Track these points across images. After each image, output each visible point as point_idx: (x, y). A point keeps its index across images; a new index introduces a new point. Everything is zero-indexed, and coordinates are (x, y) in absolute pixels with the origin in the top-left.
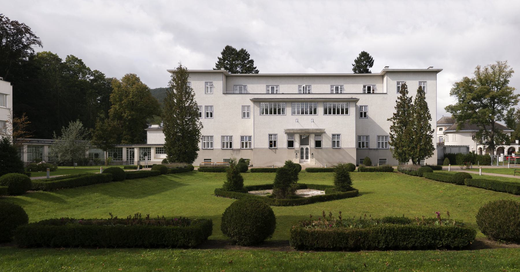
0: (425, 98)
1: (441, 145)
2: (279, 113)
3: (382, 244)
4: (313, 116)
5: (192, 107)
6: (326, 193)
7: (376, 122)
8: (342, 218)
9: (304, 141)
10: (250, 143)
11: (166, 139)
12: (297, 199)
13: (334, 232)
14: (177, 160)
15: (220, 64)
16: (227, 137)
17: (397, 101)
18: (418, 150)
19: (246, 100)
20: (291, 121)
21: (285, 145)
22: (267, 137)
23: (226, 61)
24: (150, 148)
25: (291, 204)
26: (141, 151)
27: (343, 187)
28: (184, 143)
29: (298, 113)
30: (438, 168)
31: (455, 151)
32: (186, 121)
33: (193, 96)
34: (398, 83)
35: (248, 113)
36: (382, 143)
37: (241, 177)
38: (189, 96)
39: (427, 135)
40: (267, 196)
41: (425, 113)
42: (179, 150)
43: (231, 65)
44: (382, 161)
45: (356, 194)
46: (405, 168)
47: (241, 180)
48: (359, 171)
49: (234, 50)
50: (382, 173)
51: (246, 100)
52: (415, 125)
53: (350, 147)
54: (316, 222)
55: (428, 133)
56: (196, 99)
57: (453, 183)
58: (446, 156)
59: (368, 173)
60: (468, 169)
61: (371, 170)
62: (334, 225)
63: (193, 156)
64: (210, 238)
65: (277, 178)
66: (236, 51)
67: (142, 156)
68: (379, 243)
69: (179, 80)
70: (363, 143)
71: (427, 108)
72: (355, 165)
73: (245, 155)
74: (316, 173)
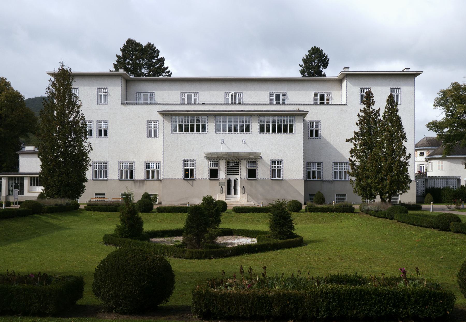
0: (397, 111)
1: (421, 175)
2: (198, 131)
3: (322, 313)
4: (244, 136)
5: (78, 121)
6: (258, 241)
7: (332, 144)
8: (268, 275)
9: (232, 169)
10: (158, 172)
11: (42, 166)
12: (216, 250)
13: (253, 295)
14: (57, 194)
15: (121, 63)
16: (127, 163)
17: (359, 115)
18: (388, 182)
19: (153, 113)
20: (216, 141)
21: (206, 175)
22: (182, 163)
23: (128, 61)
24: (22, 178)
25: (208, 256)
26: (11, 183)
27: (281, 233)
28: (67, 171)
29: (224, 131)
30: (416, 207)
31: (441, 185)
32: (69, 142)
33: (79, 107)
34: (362, 90)
35: (155, 131)
36: (340, 172)
37: (140, 218)
38: (74, 107)
39: (400, 162)
40: (174, 246)
41: (398, 131)
42: (59, 181)
43: (134, 64)
44: (340, 197)
45: (300, 243)
46: (369, 207)
47: (140, 223)
48: (306, 211)
49: (138, 45)
50: (338, 214)
51: (153, 113)
52: (384, 148)
54: (231, 281)
55: (402, 159)
56: (83, 111)
57: (434, 228)
58: (428, 191)
59: (319, 214)
60: (459, 209)
61: (323, 210)
62: (255, 286)
63: (78, 188)
64: (79, 302)
65: (190, 220)
66: (141, 46)
67: (11, 189)
68: (318, 311)
69: (60, 86)
70: (314, 172)
71: (401, 125)
72: (303, 203)
73: (151, 188)
74: (247, 214)
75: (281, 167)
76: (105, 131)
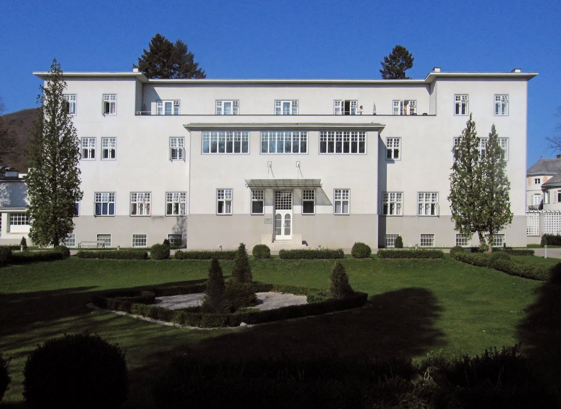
4: (300, 156)
19: (176, 126)
21: (247, 208)
22: (214, 194)
53: (211, 213)
75: (347, 198)
76: (113, 152)
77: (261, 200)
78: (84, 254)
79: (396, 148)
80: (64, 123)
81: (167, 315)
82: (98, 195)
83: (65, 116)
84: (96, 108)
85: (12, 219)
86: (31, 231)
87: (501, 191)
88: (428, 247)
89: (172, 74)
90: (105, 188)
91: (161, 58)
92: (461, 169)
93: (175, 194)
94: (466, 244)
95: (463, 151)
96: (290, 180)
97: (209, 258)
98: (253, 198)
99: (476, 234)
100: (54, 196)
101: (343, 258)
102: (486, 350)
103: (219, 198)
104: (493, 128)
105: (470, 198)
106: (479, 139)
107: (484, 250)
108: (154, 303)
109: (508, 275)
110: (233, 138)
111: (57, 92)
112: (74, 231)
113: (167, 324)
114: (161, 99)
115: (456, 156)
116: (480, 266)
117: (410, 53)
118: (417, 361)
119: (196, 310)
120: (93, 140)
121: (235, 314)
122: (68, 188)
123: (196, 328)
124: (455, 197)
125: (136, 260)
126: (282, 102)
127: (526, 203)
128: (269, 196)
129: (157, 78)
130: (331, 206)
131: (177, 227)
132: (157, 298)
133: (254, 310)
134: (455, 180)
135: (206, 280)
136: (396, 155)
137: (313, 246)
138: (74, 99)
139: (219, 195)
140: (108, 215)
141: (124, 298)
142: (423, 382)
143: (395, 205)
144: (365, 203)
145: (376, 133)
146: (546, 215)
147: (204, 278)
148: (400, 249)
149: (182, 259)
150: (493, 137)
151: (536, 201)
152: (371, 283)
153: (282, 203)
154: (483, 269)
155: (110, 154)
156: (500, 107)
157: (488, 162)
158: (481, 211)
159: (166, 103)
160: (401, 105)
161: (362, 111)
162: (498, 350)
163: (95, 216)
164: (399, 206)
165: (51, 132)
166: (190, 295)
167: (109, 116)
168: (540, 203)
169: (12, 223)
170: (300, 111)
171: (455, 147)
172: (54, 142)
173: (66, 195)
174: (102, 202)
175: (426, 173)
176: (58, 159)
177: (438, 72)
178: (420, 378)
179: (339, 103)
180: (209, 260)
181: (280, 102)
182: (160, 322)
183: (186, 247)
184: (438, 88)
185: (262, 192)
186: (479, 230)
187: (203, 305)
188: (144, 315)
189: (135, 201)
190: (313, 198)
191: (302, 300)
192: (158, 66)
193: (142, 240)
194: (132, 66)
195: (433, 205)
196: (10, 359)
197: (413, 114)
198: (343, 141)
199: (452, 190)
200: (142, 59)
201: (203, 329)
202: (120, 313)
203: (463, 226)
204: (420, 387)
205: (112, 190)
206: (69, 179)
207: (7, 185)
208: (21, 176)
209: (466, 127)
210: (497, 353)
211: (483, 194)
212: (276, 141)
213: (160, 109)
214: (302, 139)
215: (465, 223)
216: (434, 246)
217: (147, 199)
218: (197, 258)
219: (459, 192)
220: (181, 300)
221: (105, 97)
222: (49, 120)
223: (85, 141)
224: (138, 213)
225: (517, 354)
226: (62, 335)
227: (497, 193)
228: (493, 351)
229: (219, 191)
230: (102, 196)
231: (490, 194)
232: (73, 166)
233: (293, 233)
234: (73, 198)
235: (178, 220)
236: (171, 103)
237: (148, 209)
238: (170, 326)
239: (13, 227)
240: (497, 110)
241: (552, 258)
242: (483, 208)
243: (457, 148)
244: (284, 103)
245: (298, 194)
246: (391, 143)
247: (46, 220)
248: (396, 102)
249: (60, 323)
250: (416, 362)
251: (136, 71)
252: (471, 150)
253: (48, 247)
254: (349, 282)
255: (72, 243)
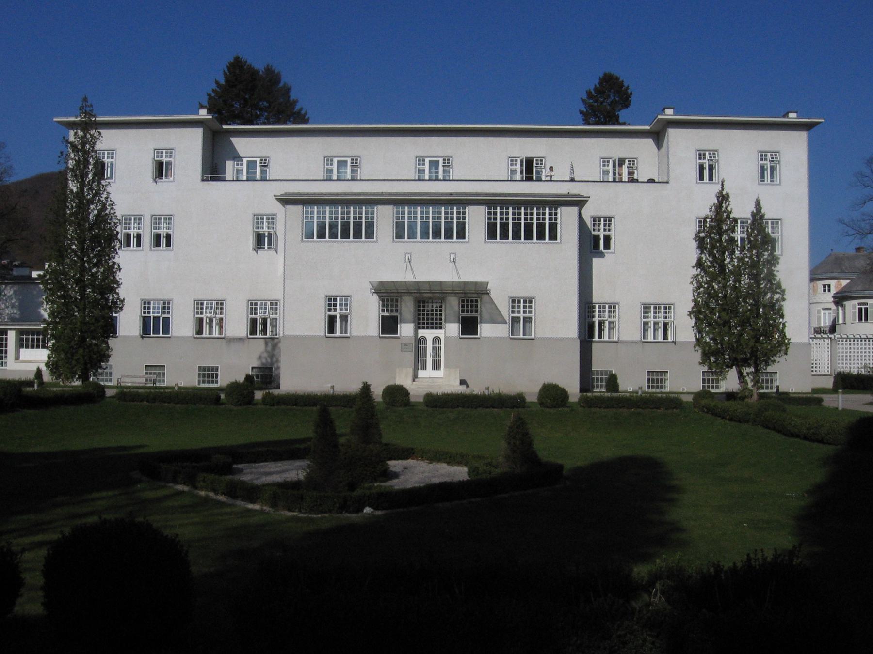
4: (454, 246)
19: (263, 197)
21: (373, 327)
22: (322, 304)
75: (530, 312)
76: (168, 237)
77: (394, 314)
78: (127, 395)
79: (607, 233)
80: (98, 194)
81: (251, 493)
82: (146, 305)
83: (99, 183)
84: (145, 171)
85: (22, 340)
86: (49, 358)
87: (771, 302)
88: (658, 391)
89: (258, 117)
90: (157, 293)
91: (242, 93)
92: (710, 267)
93: (261, 304)
94: (717, 387)
95: (712, 239)
96: (441, 283)
97: (315, 405)
98: (383, 311)
99: (733, 373)
100: (81, 306)
101: (524, 407)
102: (748, 555)
103: (330, 310)
104: (758, 204)
105: (723, 314)
106: (735, 220)
107: (746, 397)
108: (231, 474)
109: (784, 437)
110: (352, 215)
111: (88, 146)
112: (110, 359)
113: (251, 506)
114: (241, 155)
115: (701, 246)
116: (739, 422)
117: (626, 84)
118: (641, 571)
119: (295, 485)
120: (139, 219)
121: (355, 493)
122: (102, 294)
123: (296, 513)
124: (700, 312)
125: (203, 406)
126: (427, 160)
127: (810, 323)
128: (407, 307)
129: (234, 123)
130: (505, 325)
131: (265, 355)
132: (235, 466)
133: (385, 487)
134: (700, 286)
135: (309, 439)
136: (607, 245)
137: (477, 388)
138: (112, 158)
139: (330, 305)
140: (161, 335)
141: (185, 464)
142: (649, 604)
143: (607, 323)
144: (559, 321)
145: (575, 210)
146: (841, 342)
147: (307, 436)
148: (615, 395)
149: (273, 405)
150: (758, 217)
151: (825, 320)
152: (568, 448)
153: (428, 319)
154: (745, 426)
155: (163, 241)
156: (768, 169)
157: (750, 258)
158: (740, 335)
159: (248, 162)
160: (614, 166)
161: (552, 174)
162: (766, 555)
163: (142, 337)
164: (612, 325)
165: (78, 207)
166: (285, 462)
167: (163, 183)
168: (831, 323)
169: (22, 346)
170: (455, 173)
171: (699, 232)
172: (82, 223)
173: (99, 304)
174: (151, 315)
175: (653, 276)
176: (87, 249)
177: (669, 114)
178: (646, 597)
179: (516, 161)
180: (315, 408)
181: (424, 160)
182: (241, 504)
183: (278, 387)
184: (671, 139)
185: (397, 301)
186: (737, 366)
187: (305, 478)
188: (216, 491)
189: (202, 313)
190: (476, 312)
191: (460, 473)
192: (237, 105)
193: (213, 374)
194: (198, 106)
195: (665, 325)
196: (23, 551)
197: (632, 180)
198: (523, 222)
199: (695, 301)
200: (213, 95)
201: (306, 515)
202: (180, 487)
203: (712, 359)
204: (645, 612)
205: (166, 297)
206: (103, 280)
207: (16, 287)
208: (34, 274)
209: (716, 202)
210: (765, 559)
211: (744, 307)
212: (419, 221)
213: (239, 172)
214: (458, 218)
215: (716, 353)
216: (668, 390)
217: (218, 311)
218: (296, 405)
219: (706, 304)
220: (272, 470)
221: (158, 153)
222: (75, 190)
223: (127, 221)
224: (206, 334)
225: (796, 561)
226: (94, 519)
227: (764, 306)
228: (759, 556)
229: (330, 300)
230: (152, 306)
231: (754, 308)
232: (110, 259)
233: (446, 367)
234: (110, 308)
235: (266, 344)
236: (256, 162)
237: (221, 327)
238: (256, 510)
239: (23, 351)
240: (763, 176)
241: (850, 411)
242: (743, 330)
243: (702, 235)
244: (430, 162)
245: (453, 304)
246: (599, 225)
247: (70, 342)
248: (605, 161)
249: (93, 500)
250: (639, 573)
251: (203, 114)
252: (725, 237)
253: (73, 384)
254: (535, 446)
255: (109, 378)
